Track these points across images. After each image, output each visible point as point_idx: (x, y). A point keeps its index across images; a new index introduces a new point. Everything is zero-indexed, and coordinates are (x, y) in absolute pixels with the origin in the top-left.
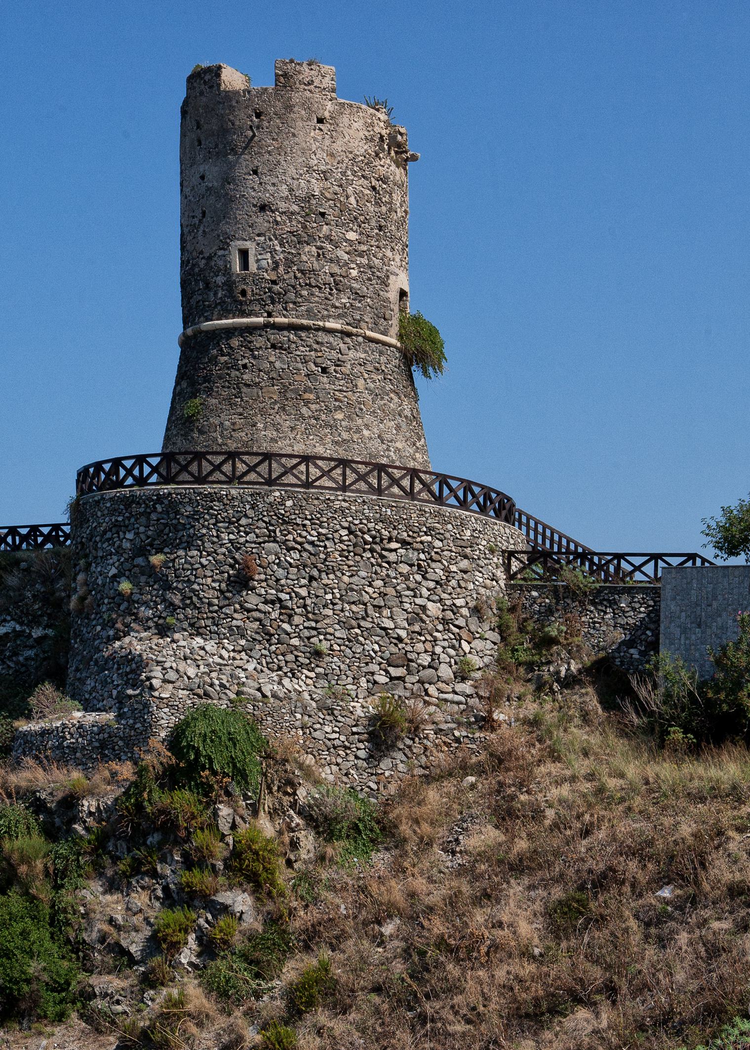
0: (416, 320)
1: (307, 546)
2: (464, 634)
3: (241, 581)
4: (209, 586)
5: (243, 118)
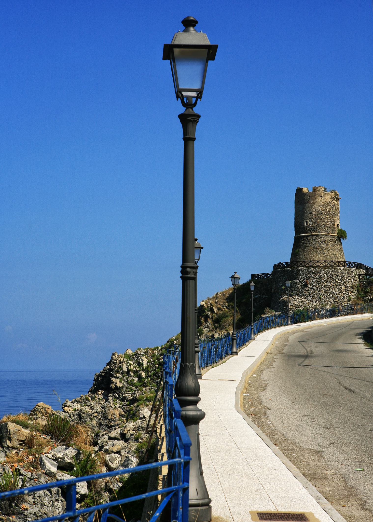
0: (341, 230)
2: (350, 292)
3: (305, 285)
4: (299, 287)
5: (307, 197)
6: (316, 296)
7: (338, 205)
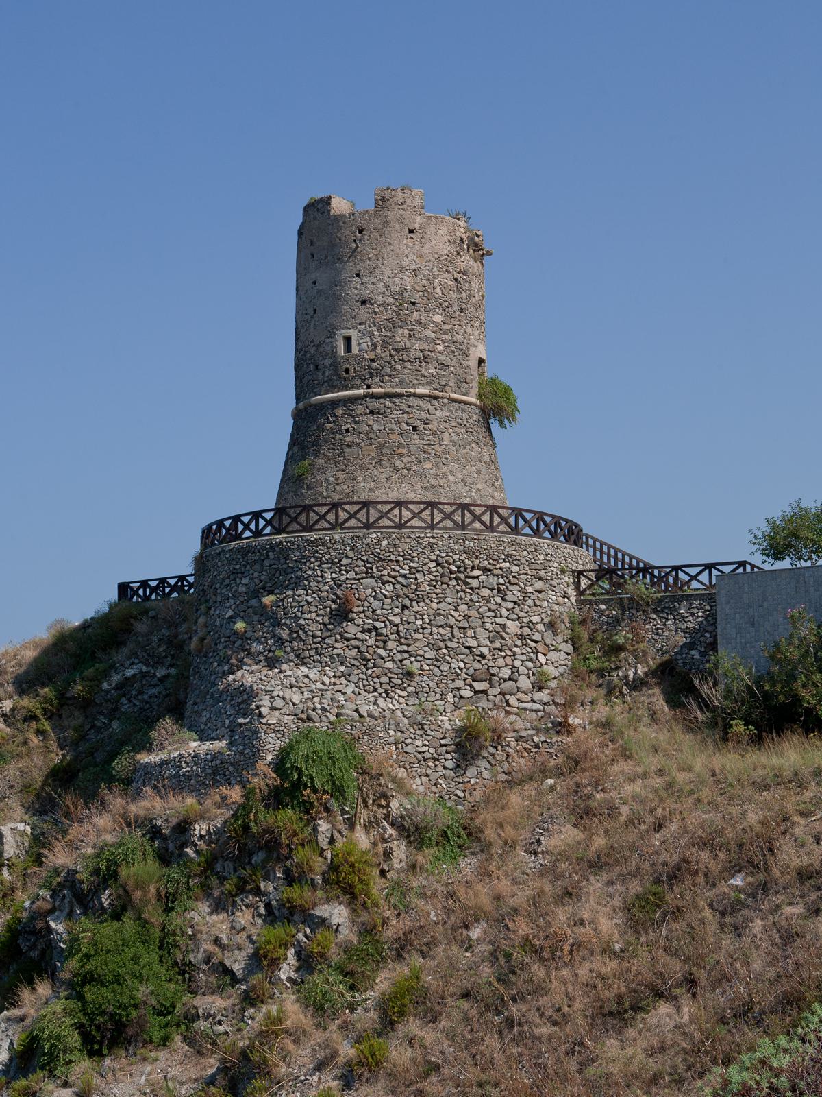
0: (493, 381)
1: (400, 579)
2: (540, 647)
3: (342, 614)
4: (313, 621)
5: (348, 234)
7: (478, 276)
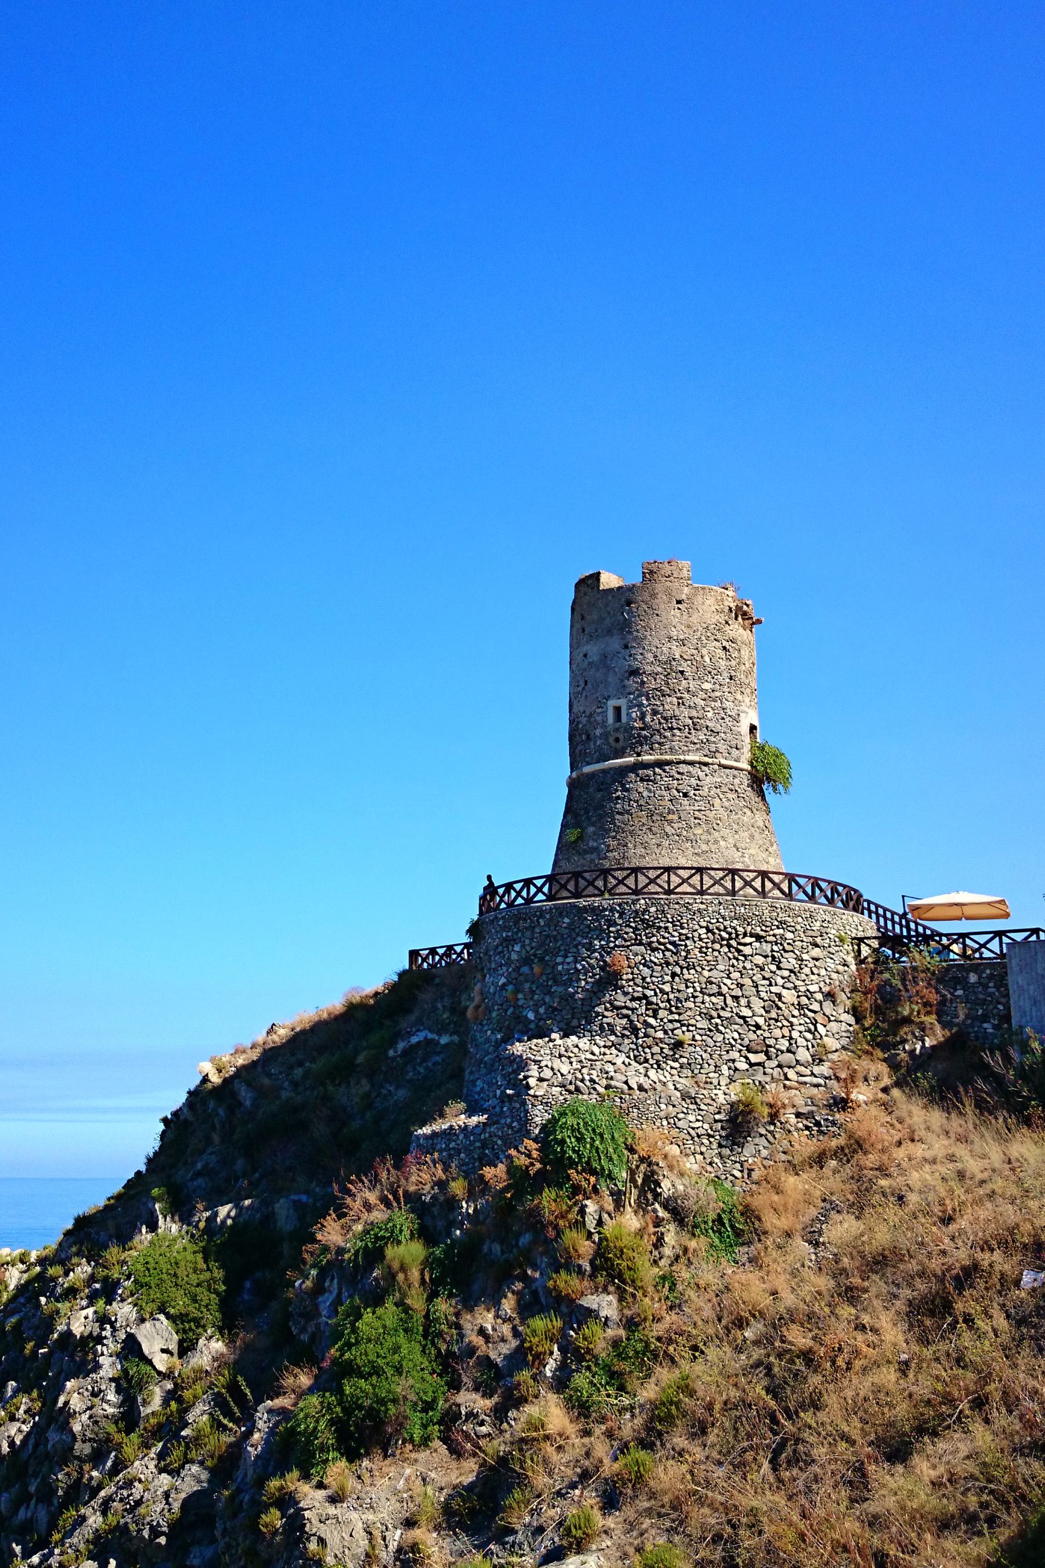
2: (820, 1018)
6: (660, 1034)
